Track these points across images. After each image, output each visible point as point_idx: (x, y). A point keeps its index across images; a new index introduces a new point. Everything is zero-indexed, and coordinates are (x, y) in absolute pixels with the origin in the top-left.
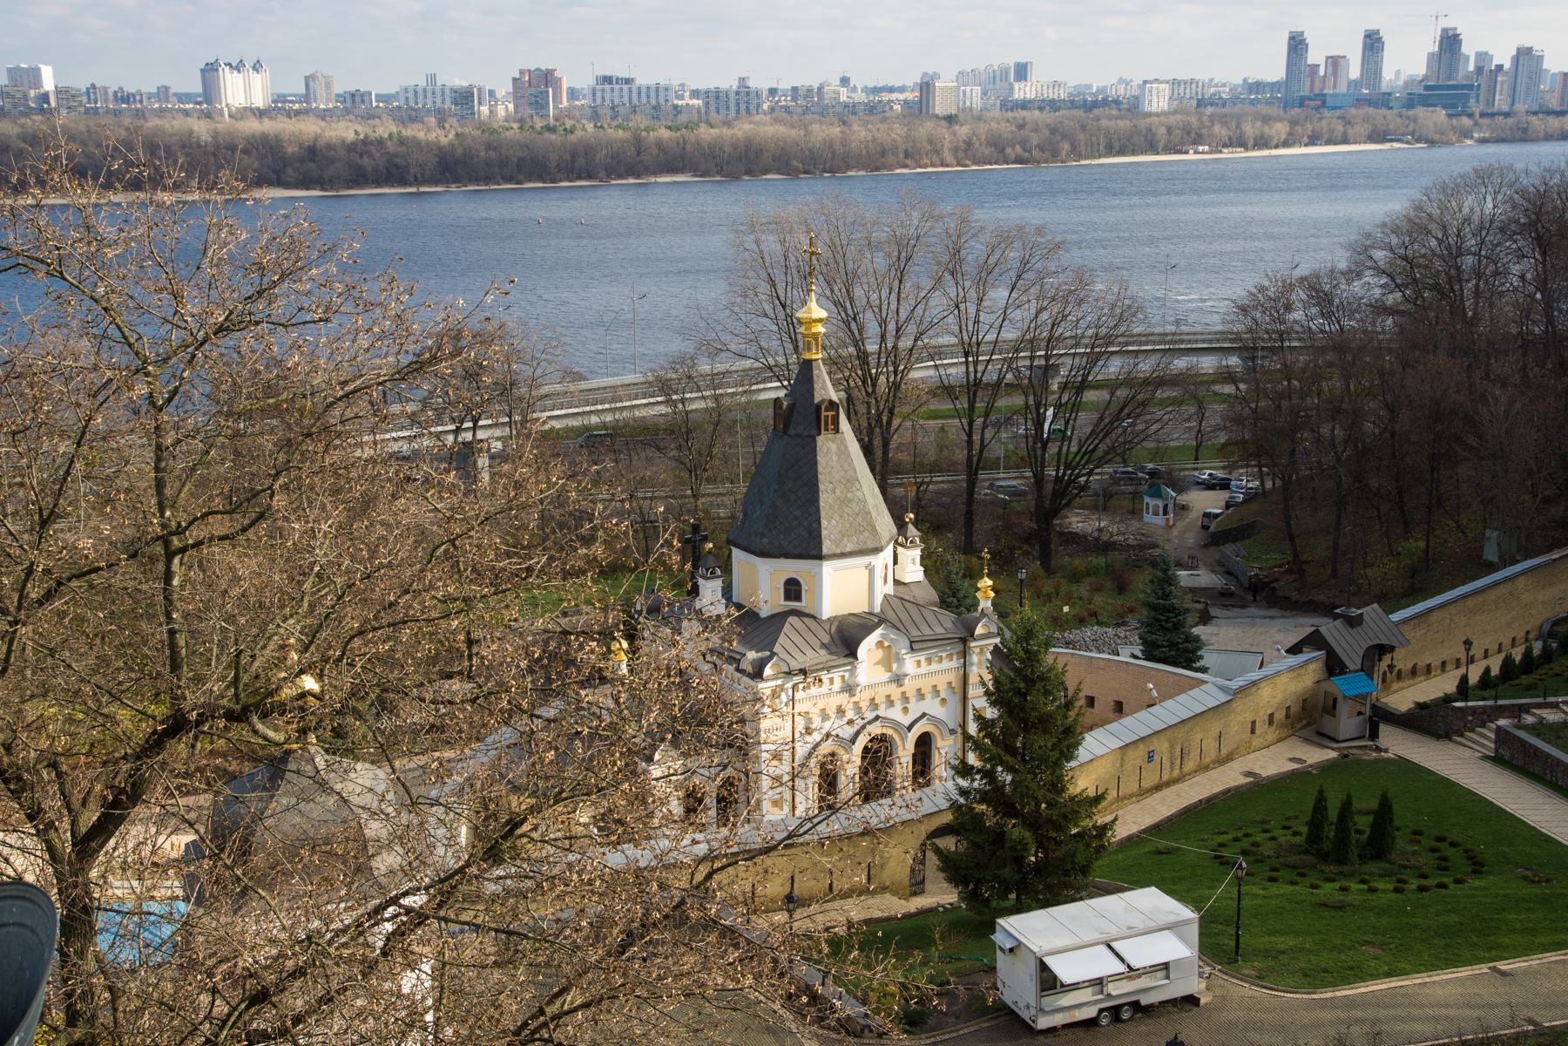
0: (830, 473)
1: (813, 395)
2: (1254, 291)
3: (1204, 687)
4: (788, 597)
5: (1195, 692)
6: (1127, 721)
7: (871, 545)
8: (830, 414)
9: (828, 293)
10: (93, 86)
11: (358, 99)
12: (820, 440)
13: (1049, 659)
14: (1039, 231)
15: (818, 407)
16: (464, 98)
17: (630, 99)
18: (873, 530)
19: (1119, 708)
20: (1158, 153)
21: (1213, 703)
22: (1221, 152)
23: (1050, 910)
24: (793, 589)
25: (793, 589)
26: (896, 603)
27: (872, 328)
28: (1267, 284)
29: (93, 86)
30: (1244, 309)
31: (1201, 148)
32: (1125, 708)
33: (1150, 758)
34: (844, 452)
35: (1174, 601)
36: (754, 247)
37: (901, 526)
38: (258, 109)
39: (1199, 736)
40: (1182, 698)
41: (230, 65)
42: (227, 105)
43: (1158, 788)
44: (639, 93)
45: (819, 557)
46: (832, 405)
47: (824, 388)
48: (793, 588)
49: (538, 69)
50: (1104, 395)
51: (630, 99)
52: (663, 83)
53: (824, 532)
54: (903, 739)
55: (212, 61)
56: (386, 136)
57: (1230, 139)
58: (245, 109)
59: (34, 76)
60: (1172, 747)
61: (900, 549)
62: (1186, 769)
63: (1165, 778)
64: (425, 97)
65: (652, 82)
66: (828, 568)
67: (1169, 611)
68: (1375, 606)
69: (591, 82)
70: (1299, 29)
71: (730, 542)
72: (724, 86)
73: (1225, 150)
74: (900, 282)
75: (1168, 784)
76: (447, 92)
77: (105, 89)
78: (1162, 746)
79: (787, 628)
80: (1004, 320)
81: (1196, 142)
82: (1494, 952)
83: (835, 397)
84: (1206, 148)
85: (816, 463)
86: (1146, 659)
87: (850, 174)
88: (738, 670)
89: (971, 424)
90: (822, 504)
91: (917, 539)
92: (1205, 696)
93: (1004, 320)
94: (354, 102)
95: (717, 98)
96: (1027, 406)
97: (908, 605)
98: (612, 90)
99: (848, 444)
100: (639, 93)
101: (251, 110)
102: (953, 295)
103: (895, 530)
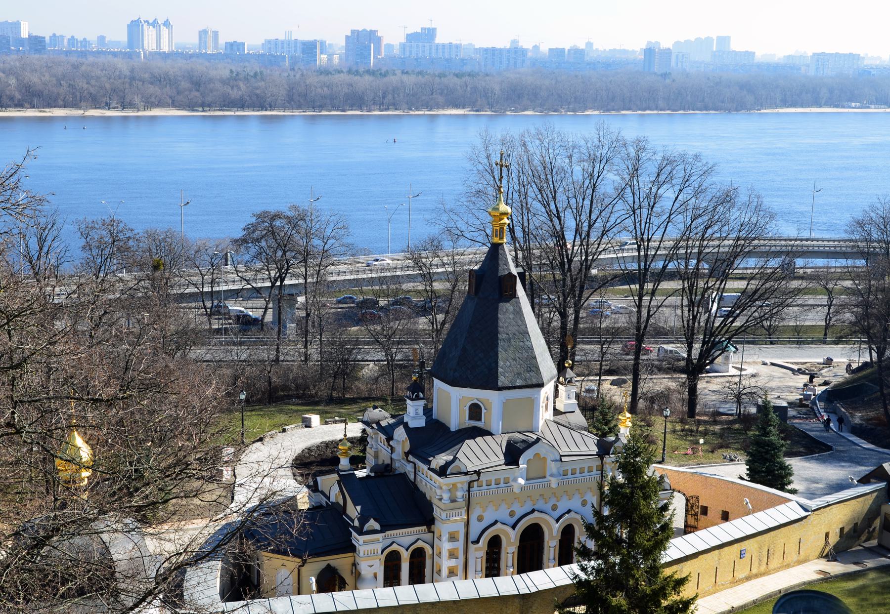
0: (507, 327)
1: (497, 269)
2: (867, 209)
3: (789, 504)
4: (471, 418)
5: (781, 507)
6: (726, 525)
7: (534, 381)
9: (539, 197)
10: (54, 35)
11: (235, 48)
13: (650, 473)
14: (697, 157)
16: (310, 48)
17: (430, 54)
19: (725, 517)
20: (821, 107)
21: (797, 517)
22: (869, 107)
23: (346, 609)
27: (570, 223)
28: (879, 206)
29: (54, 35)
30: (860, 224)
31: (853, 104)
32: (730, 516)
33: (742, 554)
35: (773, 438)
36: (486, 161)
38: (164, 53)
39: (783, 541)
40: (770, 511)
41: (147, 22)
42: (143, 49)
43: (748, 578)
44: (437, 50)
47: (507, 264)
49: (364, 30)
50: (742, 284)
51: (430, 54)
52: (454, 42)
55: (136, 19)
56: (252, 74)
57: (877, 99)
58: (156, 53)
59: (17, 26)
60: (760, 548)
61: (560, 386)
62: (772, 566)
63: (754, 571)
64: (283, 48)
65: (446, 42)
67: (768, 446)
69: (403, 40)
71: (433, 374)
72: (500, 45)
73: (873, 106)
74: (593, 191)
75: (756, 576)
76: (299, 45)
77: (62, 37)
78: (792, 556)
80: (668, 222)
81: (851, 100)
84: (858, 104)
86: (753, 480)
87: (587, 113)
88: (430, 469)
89: (640, 300)
92: (789, 510)
93: (668, 222)
94: (232, 49)
95: (493, 55)
96: (684, 289)
97: (561, 428)
98: (417, 46)
99: (523, 306)
100: (437, 50)
101: (160, 54)
102: (631, 202)
103: (555, 372)
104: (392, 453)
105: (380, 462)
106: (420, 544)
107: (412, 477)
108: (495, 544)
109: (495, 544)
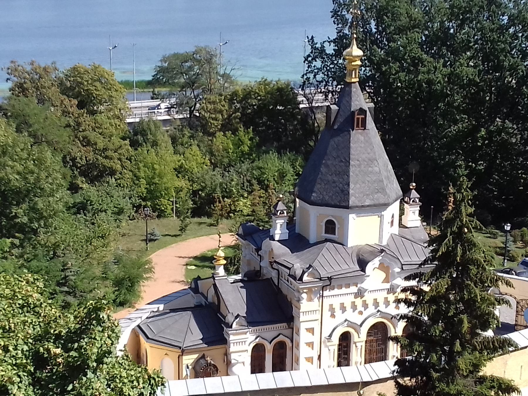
4: (327, 232)
7: (382, 201)
8: (360, 117)
12: (353, 133)
15: (353, 112)
18: (382, 190)
24: (330, 227)
25: (330, 227)
26: (398, 240)
34: (369, 142)
37: (406, 190)
45: (347, 207)
46: (362, 111)
48: (330, 226)
53: (351, 192)
54: (358, 333)
66: (352, 217)
68: (245, 290)
70: (331, 318)
79: (324, 251)
82: (367, 352)
83: (366, 107)
85: (349, 148)
90: (351, 174)
91: (417, 200)
104: (261, 261)
105: (253, 269)
106: (281, 338)
107: (276, 282)
108: (345, 338)
109: (345, 338)
